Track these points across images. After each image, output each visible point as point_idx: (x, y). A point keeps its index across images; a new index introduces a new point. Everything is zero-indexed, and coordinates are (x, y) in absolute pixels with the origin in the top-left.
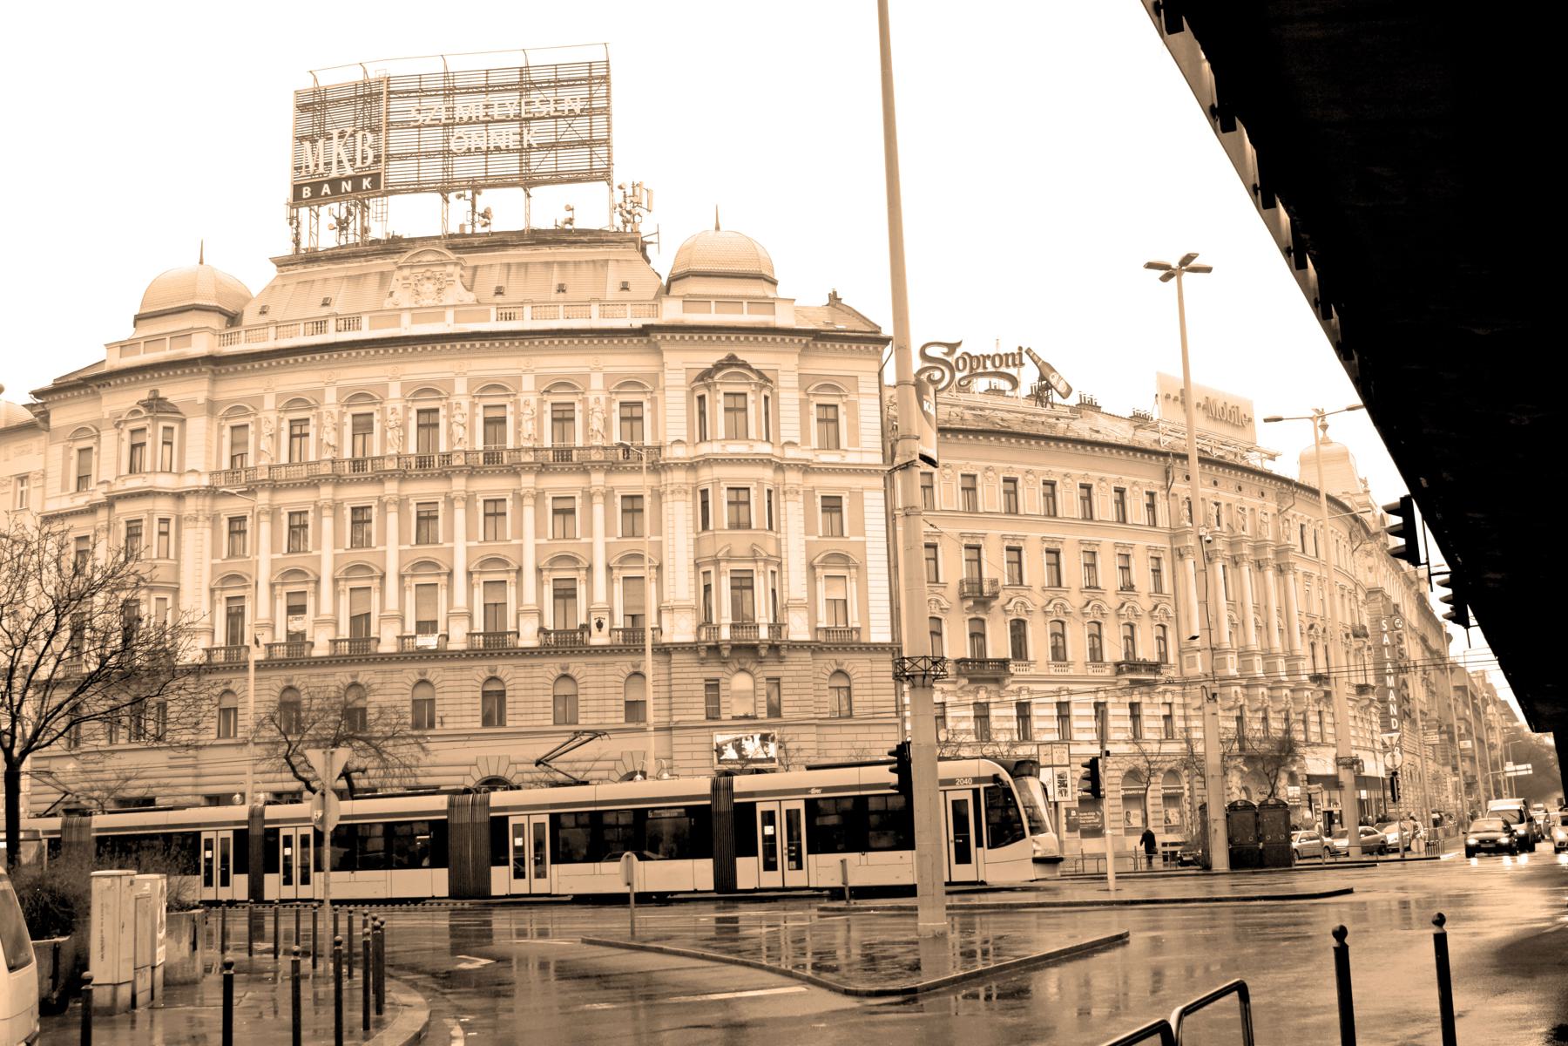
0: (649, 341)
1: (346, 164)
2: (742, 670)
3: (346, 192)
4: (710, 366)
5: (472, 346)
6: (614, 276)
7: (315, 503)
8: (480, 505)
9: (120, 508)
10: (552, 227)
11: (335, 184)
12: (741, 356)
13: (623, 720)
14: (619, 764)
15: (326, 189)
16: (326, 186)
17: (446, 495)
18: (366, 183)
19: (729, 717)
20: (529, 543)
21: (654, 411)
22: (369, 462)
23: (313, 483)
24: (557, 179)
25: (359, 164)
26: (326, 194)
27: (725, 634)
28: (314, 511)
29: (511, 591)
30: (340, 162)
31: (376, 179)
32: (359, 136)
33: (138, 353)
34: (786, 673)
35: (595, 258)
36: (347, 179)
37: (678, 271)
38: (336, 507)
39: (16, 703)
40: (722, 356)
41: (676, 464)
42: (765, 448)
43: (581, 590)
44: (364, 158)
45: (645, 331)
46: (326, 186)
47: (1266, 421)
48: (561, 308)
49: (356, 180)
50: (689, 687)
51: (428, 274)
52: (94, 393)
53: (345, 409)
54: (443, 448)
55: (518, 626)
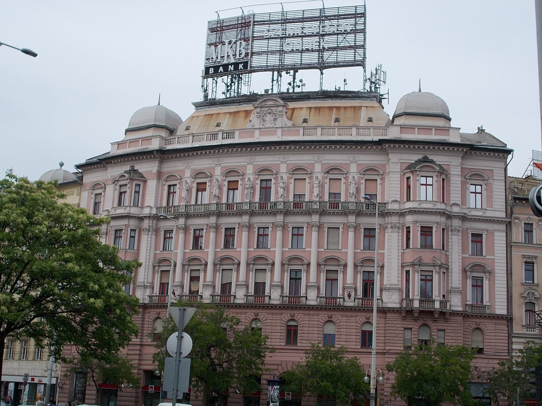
1: (231, 57)
3: (231, 70)
11: (226, 67)
12: (430, 157)
13: (359, 347)
14: (280, 367)
15: (221, 69)
16: (221, 67)
18: (241, 66)
21: (382, 184)
24: (337, 65)
25: (238, 57)
27: (416, 304)
32: (238, 43)
34: (448, 328)
36: (231, 64)
42: (134, 211)
44: (240, 54)
45: (381, 142)
46: (221, 67)
47: (35, 55)
49: (236, 65)
50: (396, 332)
51: (269, 111)
52: (104, 166)
55: (306, 294)
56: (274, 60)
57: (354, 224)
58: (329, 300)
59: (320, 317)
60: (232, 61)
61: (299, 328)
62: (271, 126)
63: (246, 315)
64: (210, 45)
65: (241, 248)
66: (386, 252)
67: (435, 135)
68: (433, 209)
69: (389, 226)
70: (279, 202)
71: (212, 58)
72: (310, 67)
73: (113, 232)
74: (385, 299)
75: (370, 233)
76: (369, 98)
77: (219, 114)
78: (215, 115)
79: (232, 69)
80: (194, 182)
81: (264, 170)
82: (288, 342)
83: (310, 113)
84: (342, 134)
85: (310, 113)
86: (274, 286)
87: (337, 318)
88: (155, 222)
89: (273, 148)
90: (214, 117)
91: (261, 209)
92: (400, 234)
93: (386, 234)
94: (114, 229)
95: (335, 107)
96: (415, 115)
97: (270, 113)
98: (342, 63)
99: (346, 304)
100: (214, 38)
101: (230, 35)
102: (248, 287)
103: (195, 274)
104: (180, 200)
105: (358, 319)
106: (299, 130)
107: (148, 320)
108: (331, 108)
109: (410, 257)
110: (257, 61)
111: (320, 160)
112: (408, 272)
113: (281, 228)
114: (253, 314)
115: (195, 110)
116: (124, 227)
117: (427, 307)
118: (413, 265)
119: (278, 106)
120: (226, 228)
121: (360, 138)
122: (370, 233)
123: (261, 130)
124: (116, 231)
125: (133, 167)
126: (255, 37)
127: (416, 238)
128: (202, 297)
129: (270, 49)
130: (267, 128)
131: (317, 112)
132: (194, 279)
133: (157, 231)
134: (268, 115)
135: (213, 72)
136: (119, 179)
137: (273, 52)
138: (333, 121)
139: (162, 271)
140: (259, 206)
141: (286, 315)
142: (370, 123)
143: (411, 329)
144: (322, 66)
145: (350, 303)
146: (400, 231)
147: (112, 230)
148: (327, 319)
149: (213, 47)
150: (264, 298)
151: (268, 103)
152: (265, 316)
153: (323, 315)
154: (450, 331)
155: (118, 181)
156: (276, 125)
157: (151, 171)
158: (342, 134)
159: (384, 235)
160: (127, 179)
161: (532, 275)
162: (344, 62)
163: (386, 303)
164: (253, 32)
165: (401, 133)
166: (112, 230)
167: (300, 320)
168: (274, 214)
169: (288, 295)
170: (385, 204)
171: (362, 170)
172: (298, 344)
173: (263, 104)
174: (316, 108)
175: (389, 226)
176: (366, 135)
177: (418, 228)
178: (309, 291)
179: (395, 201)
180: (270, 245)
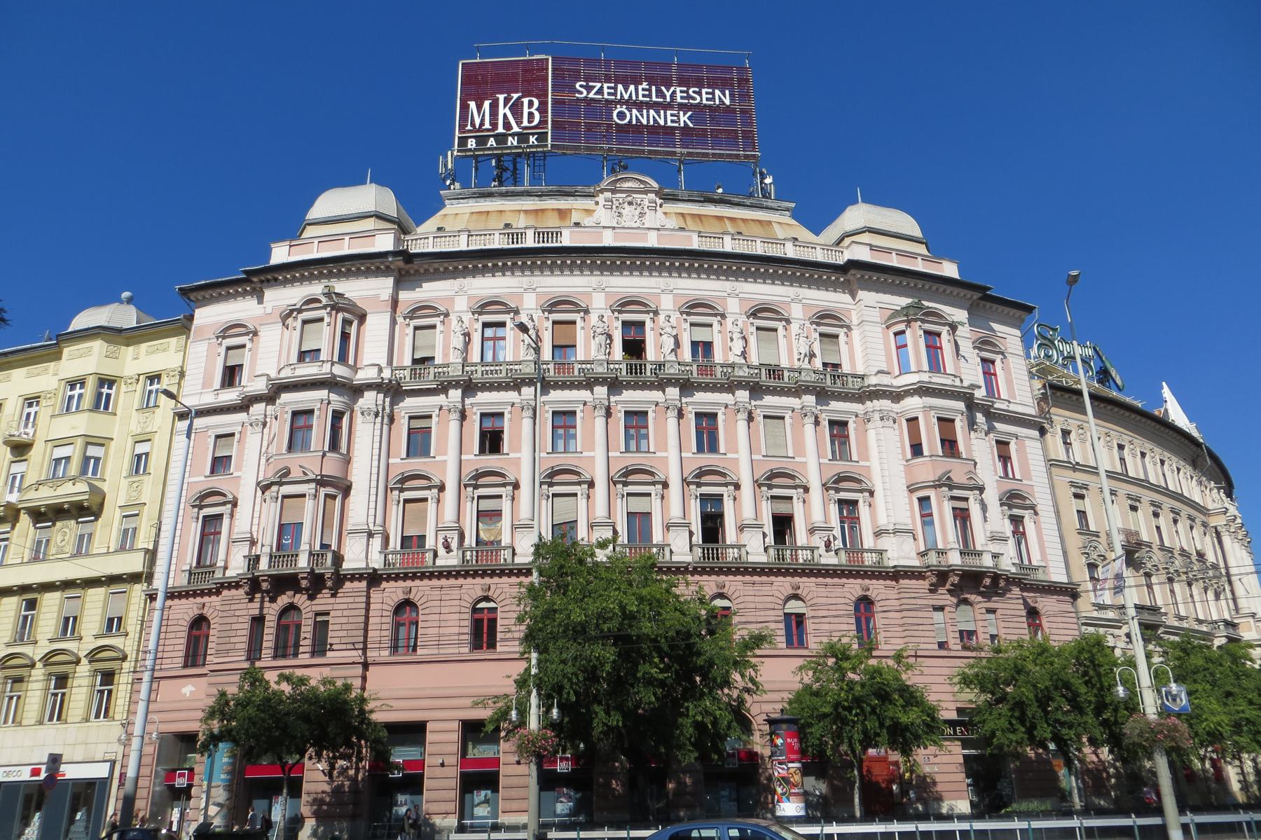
9: (285, 397)
13: (467, 650)
16: (492, 139)
19: (947, 609)
20: (599, 454)
23: (516, 384)
25: (525, 123)
34: (336, 607)
36: (513, 135)
42: (339, 370)
46: (492, 139)
51: (630, 199)
59: (774, 588)
61: (499, 615)
63: (385, 594)
65: (593, 450)
73: (289, 416)
75: (839, 427)
81: (625, 304)
82: (476, 644)
87: (500, 591)
91: (415, 378)
94: (289, 410)
95: (726, 217)
103: (486, 505)
105: (387, 594)
107: (379, 606)
109: (927, 470)
112: (924, 501)
114: (713, 585)
116: (319, 405)
117: (972, 563)
118: (937, 485)
123: (617, 231)
124: (295, 414)
127: (931, 438)
132: (488, 516)
136: (303, 308)
140: (555, 369)
141: (474, 587)
145: (448, 560)
147: (287, 412)
148: (791, 591)
150: (423, 555)
151: (637, 186)
152: (426, 593)
153: (781, 584)
154: (339, 613)
155: (300, 311)
157: (377, 296)
160: (325, 307)
161: (326, 511)
166: (287, 412)
167: (736, 594)
171: (814, 315)
172: (499, 649)
174: (693, 216)
180: (436, 450)
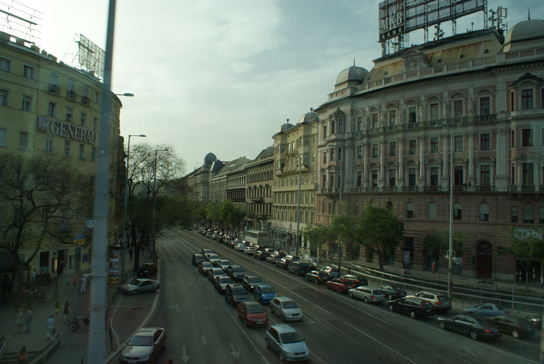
0: (491, 73)
1: (394, 25)
2: (528, 203)
3: (394, 34)
4: (517, 79)
5: (456, 78)
6: (482, 48)
7: (466, 133)
8: (479, 136)
10: (466, 32)
11: (391, 32)
12: (532, 73)
15: (389, 34)
16: (389, 33)
17: (493, 131)
18: (400, 30)
21: (494, 100)
22: (343, 133)
24: (464, 14)
25: (398, 24)
26: (389, 36)
27: (519, 189)
28: (493, 134)
29: (439, 171)
30: (392, 25)
31: (403, 27)
32: (397, 14)
33: (533, 54)
35: (476, 42)
36: (394, 30)
37: (338, 83)
38: (425, 138)
39: (132, 189)
40: (523, 74)
41: (501, 121)
43: (491, 170)
44: (399, 22)
45: (489, 69)
46: (389, 33)
48: (484, 60)
49: (397, 29)
50: (505, 209)
53: (451, 99)
54: (464, 115)
55: (494, 183)
56: (421, 20)
57: (447, 135)
58: (486, 187)
60: (395, 27)
62: (413, 70)
64: (381, 19)
66: (497, 150)
67: (536, 54)
68: (532, 115)
69: (499, 131)
70: (420, 122)
71: (383, 28)
72: (445, 20)
74: (496, 185)
75: (485, 138)
76: (487, 34)
77: (387, 65)
78: (461, 48)
79: (395, 33)
80: (370, 114)
83: (443, 54)
84: (476, 64)
85: (443, 54)
86: (443, 179)
88: (351, 141)
89: (451, 79)
90: (466, 48)
92: (508, 137)
93: (497, 138)
96: (342, 84)
97: (412, 61)
98: (468, 12)
99: (468, 190)
100: (383, 14)
101: (393, 10)
102: (426, 181)
104: (364, 128)
106: (432, 69)
108: (458, 48)
110: (412, 23)
111: (447, 89)
113: (423, 140)
115: (374, 65)
119: (417, 55)
120: (523, 130)
121: (450, 72)
122: (485, 138)
125: (338, 109)
126: (407, 7)
128: (440, 187)
129: (418, 13)
130: (411, 72)
131: (449, 52)
133: (449, 137)
134: (411, 62)
135: (384, 37)
137: (420, 15)
138: (459, 57)
139: (431, 168)
142: (486, 54)
143: (517, 207)
144: (453, 18)
146: (508, 134)
149: (383, 20)
156: (416, 68)
158: (476, 64)
159: (496, 137)
162: (471, 10)
163: (498, 188)
164: (406, 4)
165: (506, 59)
168: (419, 129)
169: (480, 185)
170: (495, 115)
172: (490, 220)
173: (407, 55)
174: (448, 50)
175: (499, 131)
176: (479, 65)
177: (520, 131)
178: (496, 181)
179: (503, 112)
